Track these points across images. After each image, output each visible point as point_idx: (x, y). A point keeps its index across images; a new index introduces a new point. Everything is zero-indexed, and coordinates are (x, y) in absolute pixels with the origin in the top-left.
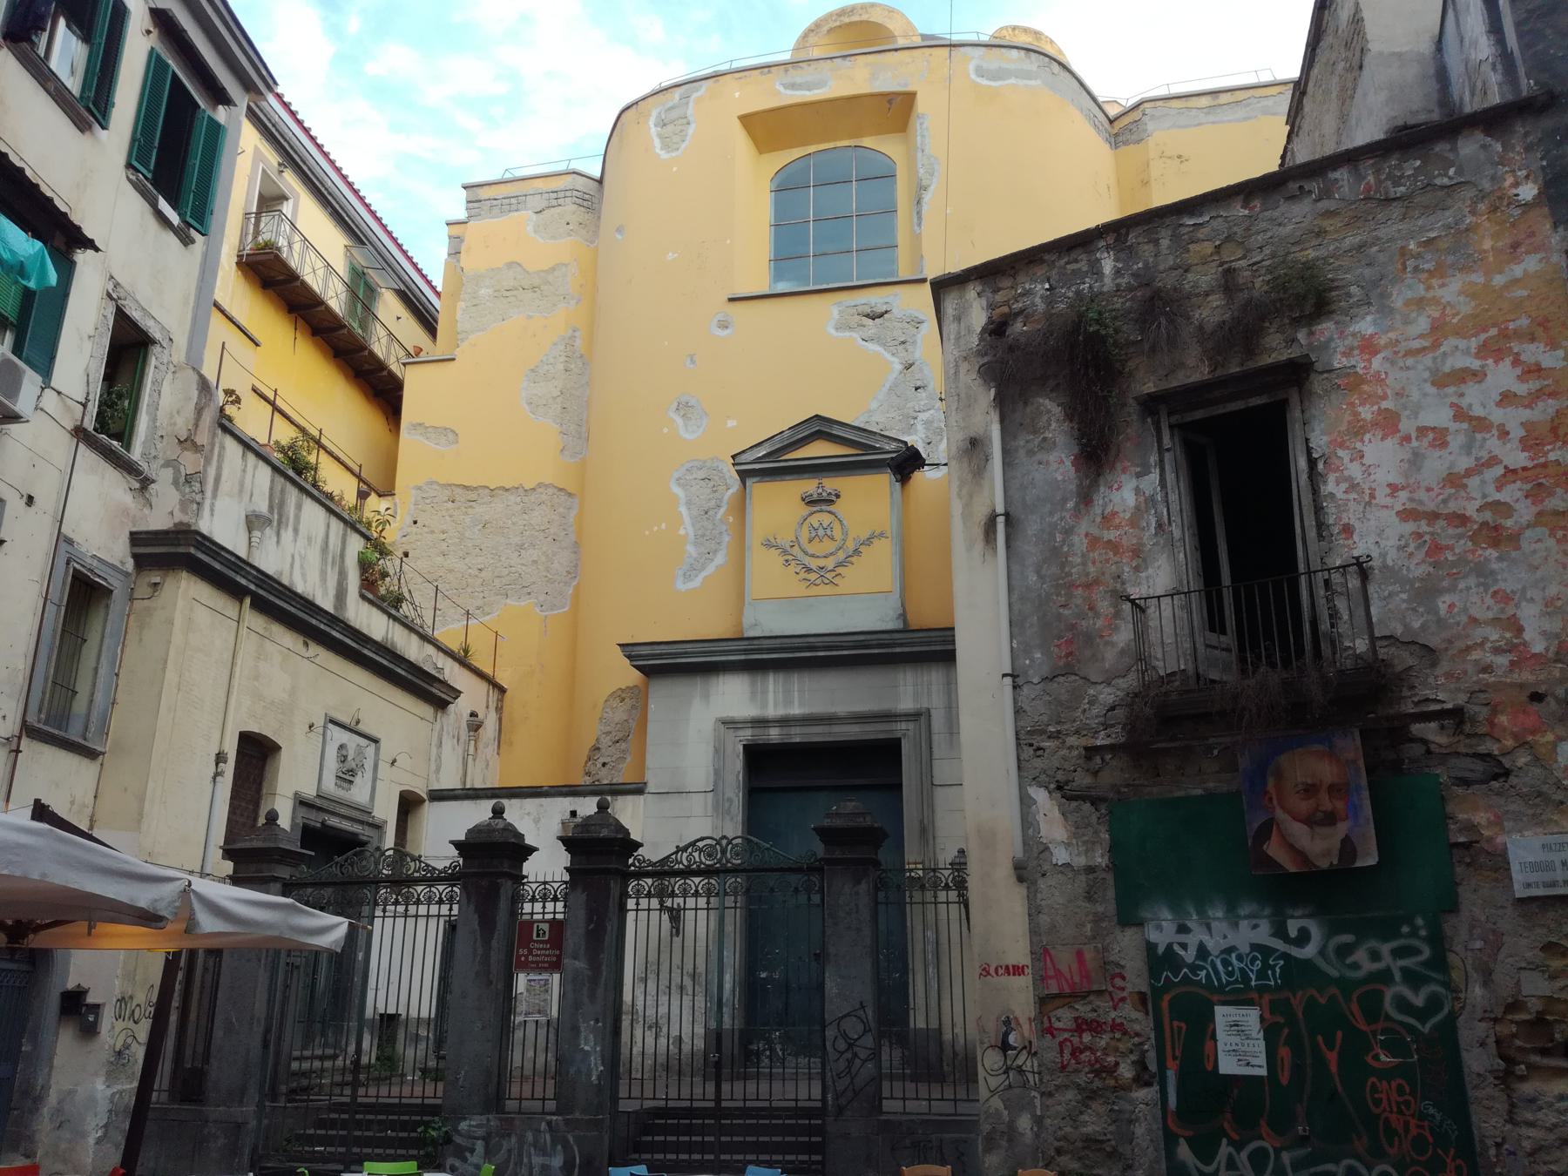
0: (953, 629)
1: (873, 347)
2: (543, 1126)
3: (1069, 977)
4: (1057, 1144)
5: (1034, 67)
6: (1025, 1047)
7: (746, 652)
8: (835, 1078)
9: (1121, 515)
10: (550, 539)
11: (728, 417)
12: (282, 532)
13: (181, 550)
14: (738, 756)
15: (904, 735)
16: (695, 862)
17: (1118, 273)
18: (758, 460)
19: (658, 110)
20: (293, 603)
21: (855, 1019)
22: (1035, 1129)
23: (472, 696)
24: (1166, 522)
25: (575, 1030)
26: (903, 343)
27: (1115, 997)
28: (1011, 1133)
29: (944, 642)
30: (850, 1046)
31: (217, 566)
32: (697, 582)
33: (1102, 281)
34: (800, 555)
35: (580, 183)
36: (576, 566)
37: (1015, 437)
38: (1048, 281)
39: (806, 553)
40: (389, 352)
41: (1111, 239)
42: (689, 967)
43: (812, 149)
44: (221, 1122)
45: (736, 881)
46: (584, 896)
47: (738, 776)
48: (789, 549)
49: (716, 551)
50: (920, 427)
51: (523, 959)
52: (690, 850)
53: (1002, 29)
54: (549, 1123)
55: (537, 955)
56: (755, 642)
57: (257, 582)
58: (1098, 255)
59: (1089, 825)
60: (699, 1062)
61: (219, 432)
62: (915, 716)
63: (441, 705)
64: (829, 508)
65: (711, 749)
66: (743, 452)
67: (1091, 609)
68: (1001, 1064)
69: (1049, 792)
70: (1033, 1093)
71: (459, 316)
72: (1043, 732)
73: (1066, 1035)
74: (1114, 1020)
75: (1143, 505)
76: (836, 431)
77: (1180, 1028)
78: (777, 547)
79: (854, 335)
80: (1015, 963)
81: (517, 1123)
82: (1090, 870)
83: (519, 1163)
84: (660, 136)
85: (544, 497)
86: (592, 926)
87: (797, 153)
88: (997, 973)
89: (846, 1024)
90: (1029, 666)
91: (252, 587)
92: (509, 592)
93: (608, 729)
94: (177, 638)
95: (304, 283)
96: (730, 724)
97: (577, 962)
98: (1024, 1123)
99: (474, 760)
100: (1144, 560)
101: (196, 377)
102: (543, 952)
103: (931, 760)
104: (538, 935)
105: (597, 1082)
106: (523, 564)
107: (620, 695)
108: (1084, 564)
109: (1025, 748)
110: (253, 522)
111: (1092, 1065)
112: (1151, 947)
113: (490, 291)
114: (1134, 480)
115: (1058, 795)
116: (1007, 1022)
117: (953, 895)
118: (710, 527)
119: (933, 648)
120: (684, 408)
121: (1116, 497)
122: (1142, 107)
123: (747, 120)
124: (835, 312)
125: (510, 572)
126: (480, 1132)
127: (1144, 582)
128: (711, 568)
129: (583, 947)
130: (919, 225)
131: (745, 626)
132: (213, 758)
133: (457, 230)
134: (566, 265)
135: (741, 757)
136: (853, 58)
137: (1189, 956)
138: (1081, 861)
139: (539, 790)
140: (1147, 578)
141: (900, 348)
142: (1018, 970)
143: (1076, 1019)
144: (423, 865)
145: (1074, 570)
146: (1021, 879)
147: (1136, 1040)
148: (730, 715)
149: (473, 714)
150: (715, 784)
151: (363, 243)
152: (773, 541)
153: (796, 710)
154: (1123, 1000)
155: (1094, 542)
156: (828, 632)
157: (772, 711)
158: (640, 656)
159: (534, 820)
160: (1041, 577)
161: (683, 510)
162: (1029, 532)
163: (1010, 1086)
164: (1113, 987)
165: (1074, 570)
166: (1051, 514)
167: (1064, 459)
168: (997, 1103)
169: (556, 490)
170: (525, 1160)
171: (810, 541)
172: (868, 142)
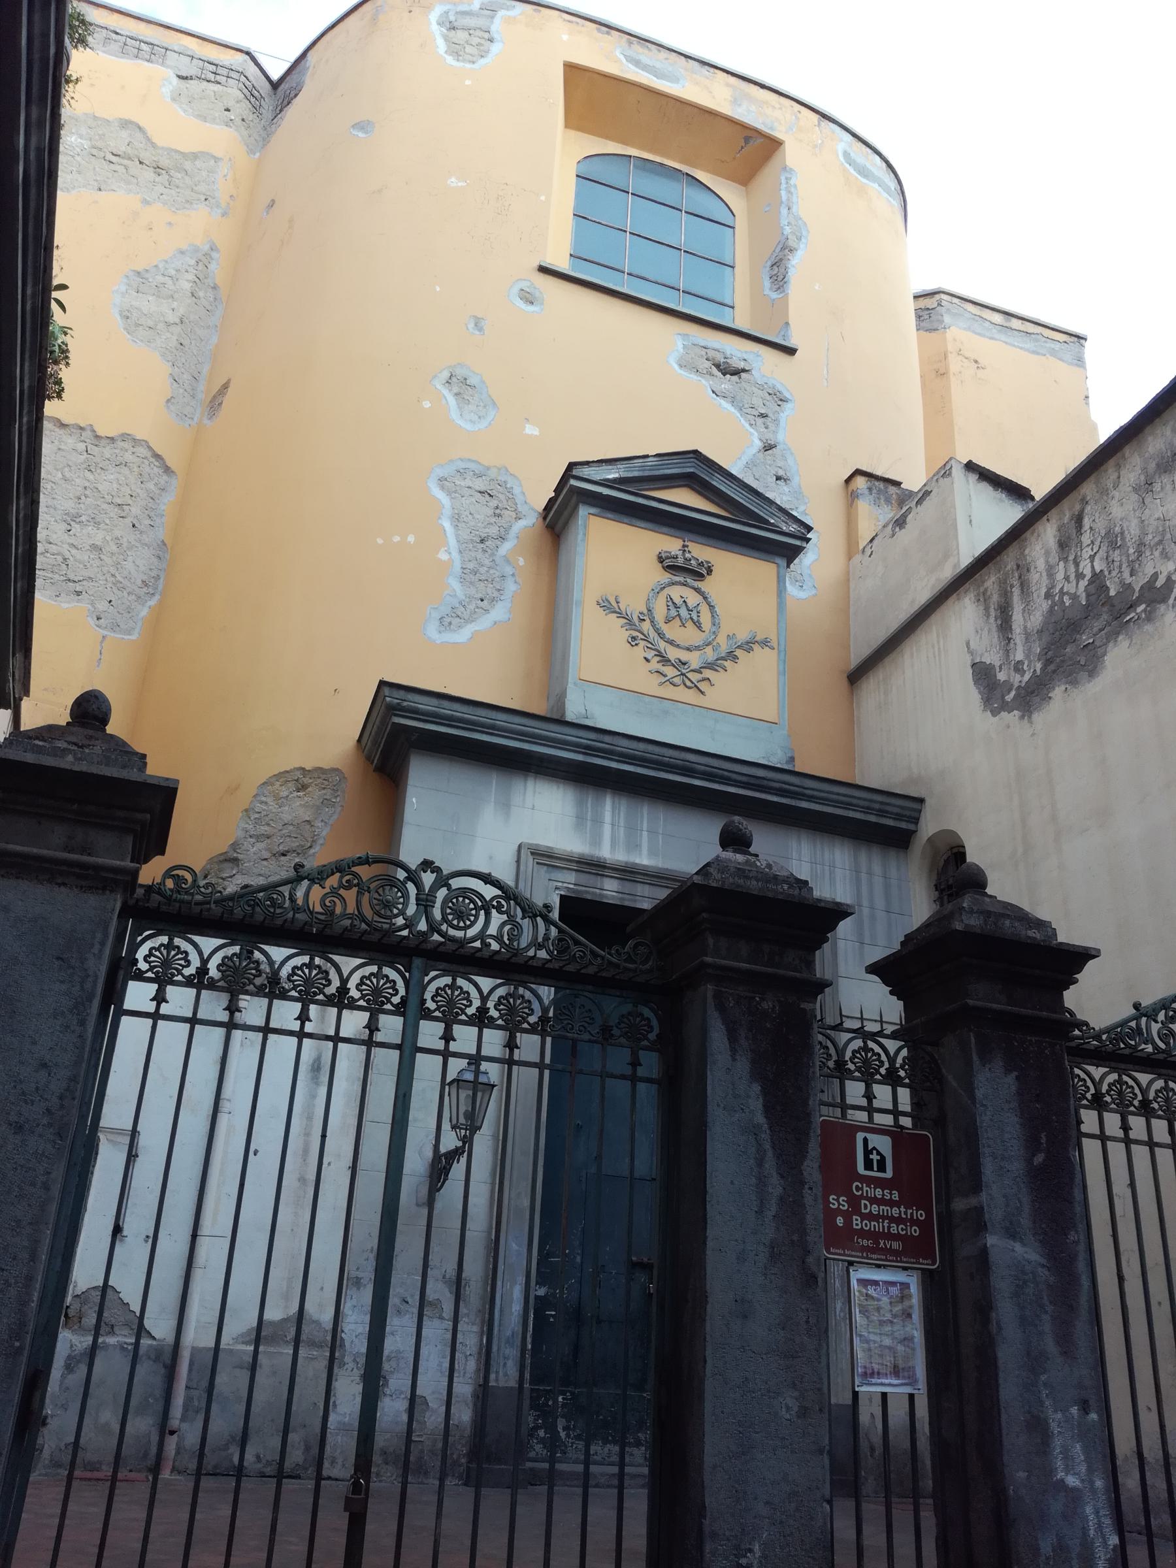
7: (588, 749)
10: (128, 521)
19: (445, 8)
32: (463, 635)
39: (661, 635)
42: (444, 1261)
49: (493, 600)
52: (333, 881)
55: (871, 1217)
56: (607, 739)
60: (460, 1451)
64: (696, 584)
66: (587, 463)
76: (717, 482)
84: (446, 39)
85: (128, 457)
86: (1039, 1159)
97: (1018, 1247)
104: (868, 1165)
106: (73, 545)
113: (86, 144)
118: (487, 562)
119: (851, 814)
122: (937, 297)
123: (571, 69)
128: (484, 623)
134: (217, 160)
136: (712, 70)
141: (760, 421)
152: (614, 603)
153: (644, 859)
157: (607, 852)
158: (416, 711)
161: (447, 525)
169: (149, 454)
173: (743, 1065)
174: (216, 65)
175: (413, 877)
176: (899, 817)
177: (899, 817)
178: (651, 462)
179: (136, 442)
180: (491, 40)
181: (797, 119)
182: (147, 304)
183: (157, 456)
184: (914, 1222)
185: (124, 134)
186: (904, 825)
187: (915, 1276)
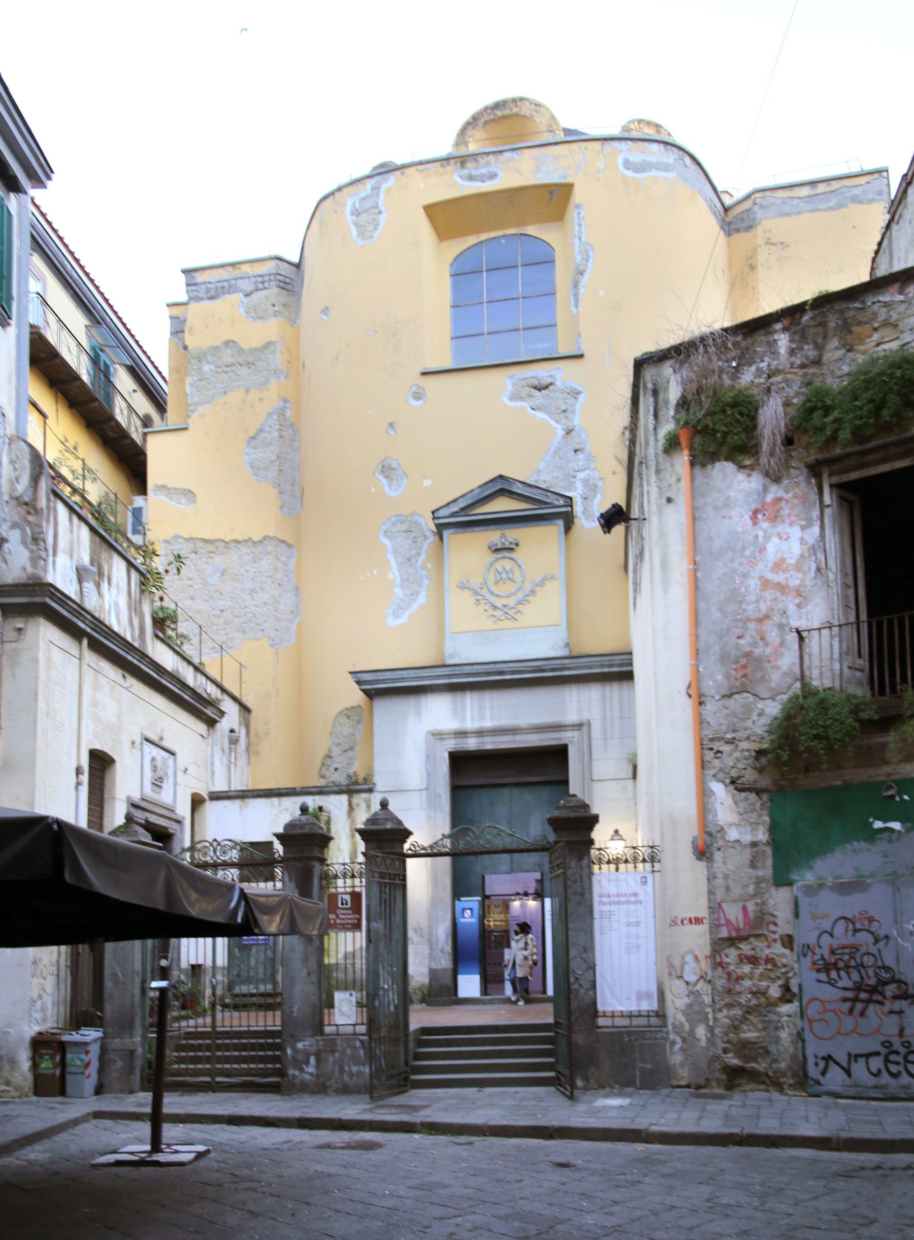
0: (631, 654)
1: (540, 415)
2: (358, 1044)
4: (724, 1045)
11: (424, 478)
13: (37, 600)
17: (792, 352)
18: (453, 515)
23: (231, 715)
24: (824, 567)
26: (565, 411)
27: (769, 939)
32: (404, 619)
33: (778, 359)
34: (488, 596)
35: (285, 269)
36: (297, 606)
39: (492, 593)
40: (129, 422)
41: (786, 322)
43: (484, 236)
48: (479, 590)
50: (579, 485)
53: (633, 121)
56: (457, 668)
57: (92, 626)
59: (755, 810)
61: (52, 497)
62: (579, 726)
63: (211, 723)
66: (442, 507)
67: (762, 639)
69: (726, 786)
71: (188, 389)
72: (720, 739)
74: (767, 955)
78: (469, 589)
79: (525, 404)
80: (696, 916)
81: (339, 1042)
82: (754, 844)
87: (472, 240)
91: (89, 630)
93: (338, 741)
94: (42, 674)
95: (63, 360)
96: (438, 736)
99: (235, 767)
101: (27, 449)
104: (342, 904)
106: (256, 606)
107: (348, 713)
110: (81, 574)
113: (212, 367)
115: (732, 788)
120: (387, 470)
122: (753, 197)
123: (431, 210)
124: (509, 384)
126: (313, 1049)
127: (804, 616)
128: (415, 607)
130: (576, 306)
131: (447, 655)
133: (176, 311)
136: (519, 152)
138: (747, 838)
140: (807, 613)
141: (562, 416)
142: (698, 921)
147: (783, 970)
149: (232, 731)
150: (428, 785)
153: (488, 724)
154: (775, 940)
155: (765, 584)
162: (715, 576)
164: (768, 931)
166: (732, 560)
172: (531, 230)
173: (293, 884)
175: (211, 845)
176: (621, 665)
177: (621, 665)
180: (380, 212)
183: (283, 541)
186: (625, 669)
187: (473, 920)
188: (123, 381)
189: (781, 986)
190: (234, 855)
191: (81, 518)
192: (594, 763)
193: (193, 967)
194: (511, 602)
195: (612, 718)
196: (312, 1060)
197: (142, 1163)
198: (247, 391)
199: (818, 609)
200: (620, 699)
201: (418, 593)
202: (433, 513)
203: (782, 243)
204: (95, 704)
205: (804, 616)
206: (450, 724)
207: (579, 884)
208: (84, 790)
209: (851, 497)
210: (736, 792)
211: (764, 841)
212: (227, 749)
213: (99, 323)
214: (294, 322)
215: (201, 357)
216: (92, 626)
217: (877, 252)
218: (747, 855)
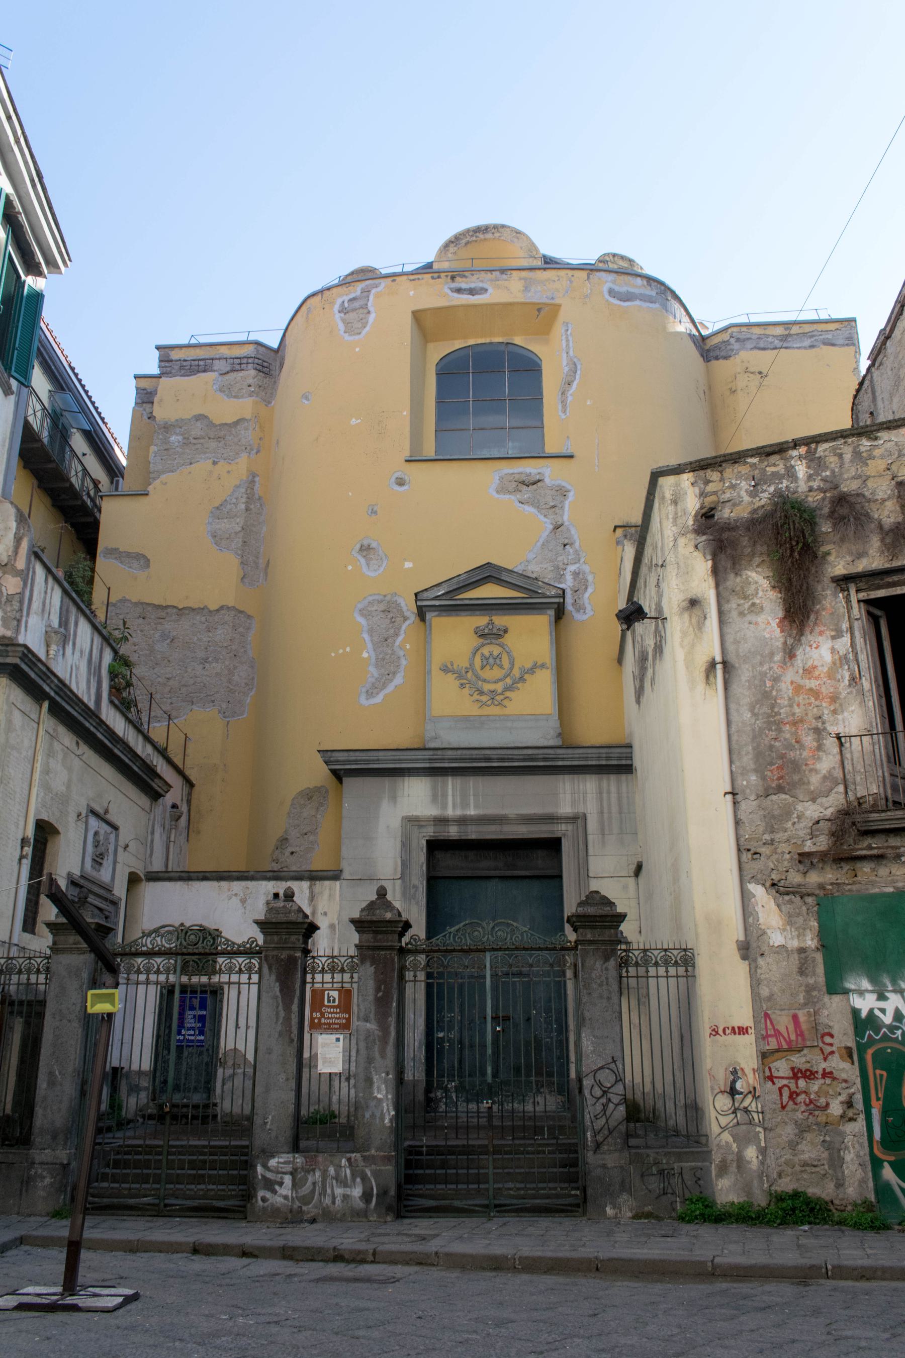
3: (786, 1035)
5: (653, 293)
6: (750, 1092)
8: (593, 1118)
9: (820, 668)
10: (231, 654)
12: (67, 646)
14: (422, 850)
15: (564, 835)
16: (157, 945)
17: (810, 477)
20: (77, 708)
21: (607, 1071)
22: (760, 1157)
25: (369, 1081)
26: (553, 507)
28: (740, 1160)
29: (627, 758)
30: (605, 1092)
31: (33, 675)
37: (728, 601)
38: (754, 479)
41: (803, 450)
44: (47, 1164)
45: (169, 962)
46: (372, 969)
47: (422, 867)
51: (316, 1021)
52: (153, 935)
53: (608, 254)
54: (349, 1160)
55: (328, 1018)
56: (439, 752)
58: (793, 462)
61: (33, 558)
63: (155, 796)
65: (399, 844)
66: (426, 590)
68: (730, 1106)
70: (758, 1129)
73: (785, 1082)
75: (838, 662)
77: (881, 1076)
78: (454, 672)
79: (513, 497)
80: (740, 1025)
82: (802, 950)
83: (324, 1193)
84: (343, 320)
86: (380, 994)
88: (725, 1034)
89: (601, 1076)
90: (747, 786)
91: (52, 694)
92: (195, 700)
96: (412, 822)
97: (368, 1025)
98: (751, 1153)
100: (841, 705)
102: (334, 1015)
103: (587, 856)
104: (329, 1001)
105: (389, 1125)
107: (309, 795)
108: (791, 706)
109: (745, 853)
110: (48, 635)
111: (807, 1105)
112: (855, 1012)
113: (180, 438)
114: (830, 641)
116: (734, 1072)
117: (681, 970)
118: (390, 652)
120: (366, 550)
121: (814, 654)
122: (730, 331)
125: (196, 682)
126: (289, 1168)
127: (841, 722)
129: (373, 1012)
130: (564, 412)
132: (19, 841)
133: (144, 384)
135: (425, 851)
137: (888, 1019)
138: (795, 944)
139: (246, 874)
142: (743, 1031)
143: (793, 1069)
144: (223, 940)
145: (782, 711)
146: (744, 958)
148: (415, 813)
150: (403, 874)
151: (63, 389)
152: (449, 666)
154: (832, 1053)
155: (798, 689)
156: (498, 746)
158: (338, 761)
159: (241, 900)
160: (755, 715)
161: (366, 636)
163: (738, 1124)
164: (824, 1043)
165: (782, 711)
166: (761, 664)
167: (771, 621)
168: (726, 1137)
170: (329, 1191)
171: (482, 669)
173: (273, 977)
174: (240, 358)
177: (620, 758)
178: (462, 578)
179: (229, 608)
180: (369, 312)
181: (571, 282)
182: (224, 526)
184: (344, 1018)
185: (199, 424)
186: (624, 762)
188: (78, 443)
189: (842, 1103)
190: (170, 944)
191: (56, 579)
192: (591, 859)
193: (115, 1070)
194: (499, 687)
195: (610, 812)
196: (288, 1180)
197: (52, 1308)
198: (215, 463)
199: (855, 716)
200: (619, 793)
201: (394, 673)
202: (416, 595)
203: (760, 373)
204: (46, 771)
205: (841, 722)
206: (429, 811)
207: (604, 987)
208: (26, 863)
209: (878, 612)
210: (778, 895)
211: (813, 946)
212: (167, 827)
213: (63, 389)
214: (270, 402)
215: (167, 428)
216: (57, 690)
217: (858, 391)
218: (795, 959)
